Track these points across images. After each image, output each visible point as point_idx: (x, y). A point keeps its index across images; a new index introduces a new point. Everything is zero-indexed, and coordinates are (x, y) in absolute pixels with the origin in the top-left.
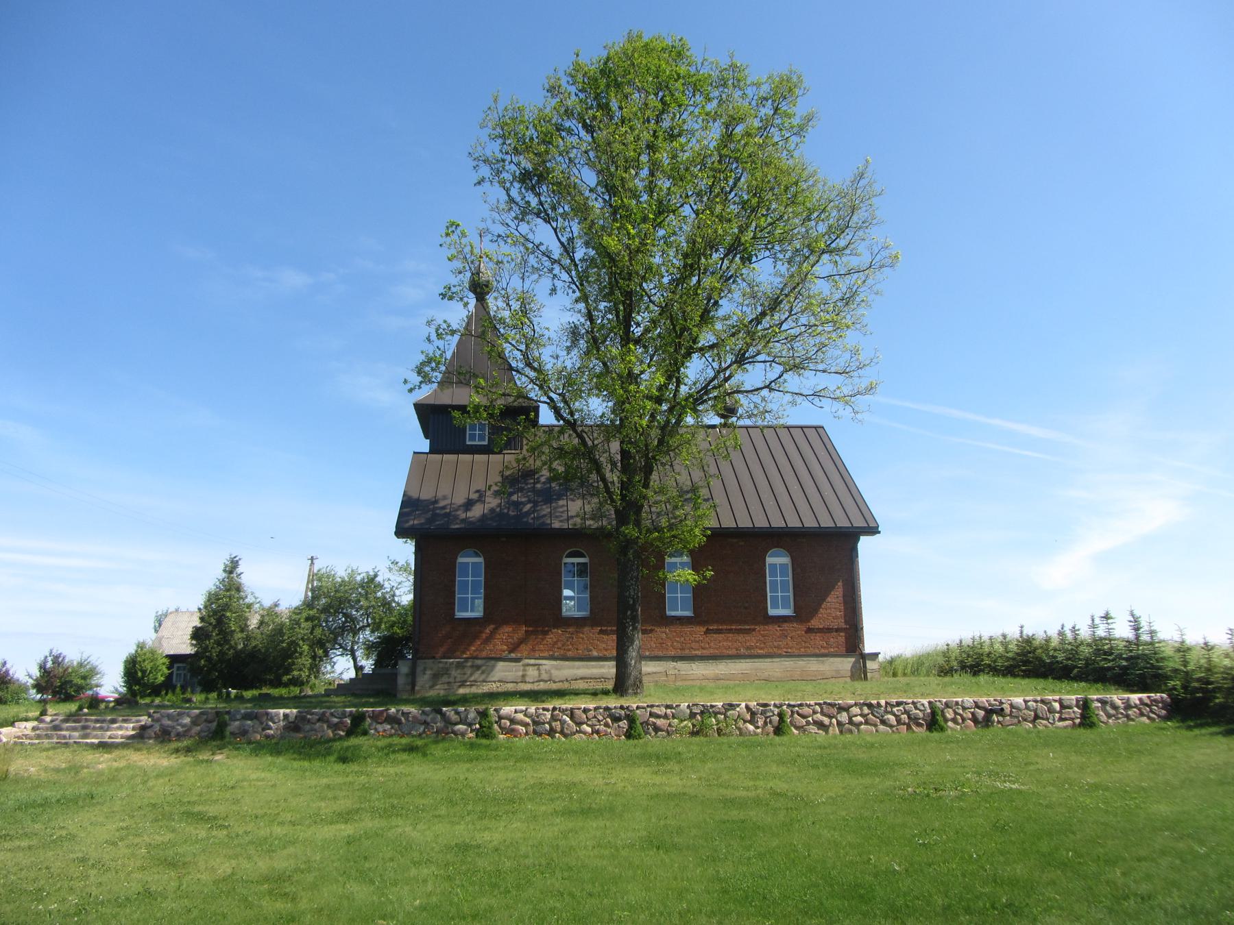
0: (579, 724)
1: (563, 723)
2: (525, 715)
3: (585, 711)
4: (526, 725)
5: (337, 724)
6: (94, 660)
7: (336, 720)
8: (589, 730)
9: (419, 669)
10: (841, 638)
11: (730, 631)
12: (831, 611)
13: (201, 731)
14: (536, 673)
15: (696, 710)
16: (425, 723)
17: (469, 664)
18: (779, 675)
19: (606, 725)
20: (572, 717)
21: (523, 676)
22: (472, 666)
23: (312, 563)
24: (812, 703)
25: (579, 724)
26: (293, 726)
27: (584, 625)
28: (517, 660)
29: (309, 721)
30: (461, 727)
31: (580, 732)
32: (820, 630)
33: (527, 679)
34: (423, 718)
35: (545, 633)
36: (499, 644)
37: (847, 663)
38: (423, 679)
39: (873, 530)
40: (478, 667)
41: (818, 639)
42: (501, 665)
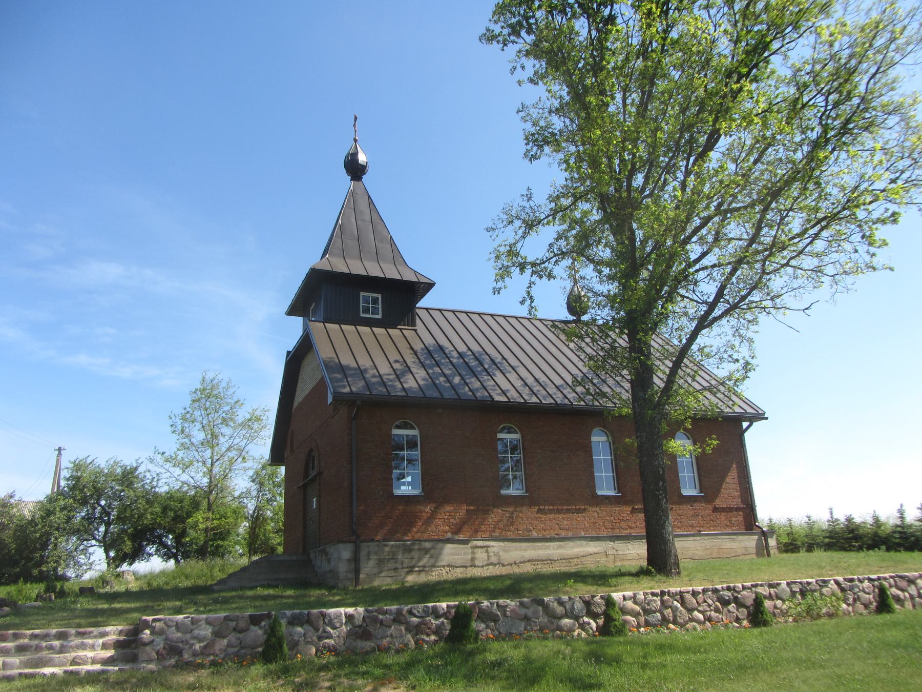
0: (690, 610)
1: (675, 609)
2: (635, 602)
3: (694, 594)
4: (636, 615)
5: (418, 626)
6: (848, 514)
7: (415, 620)
8: (701, 617)
9: (363, 553)
10: (739, 517)
11: (568, 511)
12: (729, 492)
13: (229, 645)
14: (485, 555)
15: (796, 588)
16: (526, 618)
17: (416, 547)
18: (700, 553)
19: (717, 610)
20: (683, 602)
21: (473, 559)
22: (420, 549)
23: (60, 454)
24: (887, 575)
25: (690, 610)
26: (360, 631)
27: (522, 505)
28: (465, 542)
29: (381, 622)
30: (567, 622)
31: (692, 620)
32: (723, 510)
33: (477, 563)
34: (523, 611)
35: (487, 512)
36: (441, 526)
37: (750, 541)
38: (368, 567)
39: (760, 416)
40: (427, 551)
41: (722, 518)
42: (449, 547)
